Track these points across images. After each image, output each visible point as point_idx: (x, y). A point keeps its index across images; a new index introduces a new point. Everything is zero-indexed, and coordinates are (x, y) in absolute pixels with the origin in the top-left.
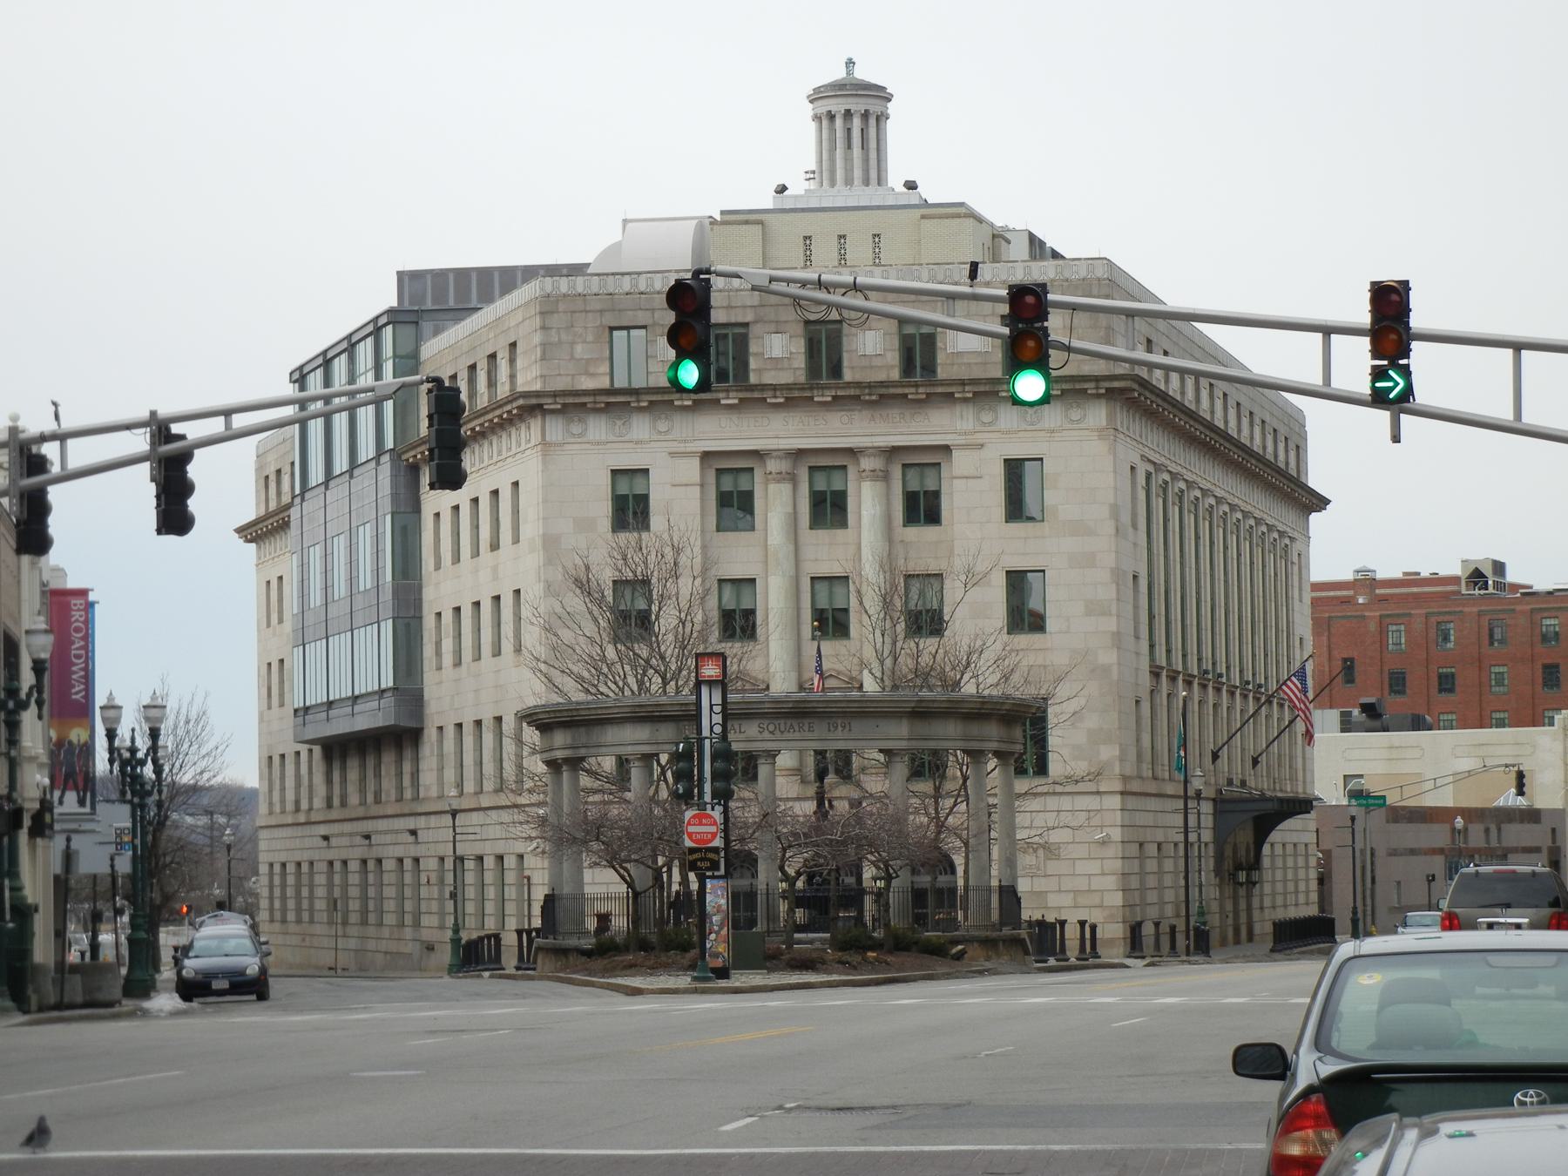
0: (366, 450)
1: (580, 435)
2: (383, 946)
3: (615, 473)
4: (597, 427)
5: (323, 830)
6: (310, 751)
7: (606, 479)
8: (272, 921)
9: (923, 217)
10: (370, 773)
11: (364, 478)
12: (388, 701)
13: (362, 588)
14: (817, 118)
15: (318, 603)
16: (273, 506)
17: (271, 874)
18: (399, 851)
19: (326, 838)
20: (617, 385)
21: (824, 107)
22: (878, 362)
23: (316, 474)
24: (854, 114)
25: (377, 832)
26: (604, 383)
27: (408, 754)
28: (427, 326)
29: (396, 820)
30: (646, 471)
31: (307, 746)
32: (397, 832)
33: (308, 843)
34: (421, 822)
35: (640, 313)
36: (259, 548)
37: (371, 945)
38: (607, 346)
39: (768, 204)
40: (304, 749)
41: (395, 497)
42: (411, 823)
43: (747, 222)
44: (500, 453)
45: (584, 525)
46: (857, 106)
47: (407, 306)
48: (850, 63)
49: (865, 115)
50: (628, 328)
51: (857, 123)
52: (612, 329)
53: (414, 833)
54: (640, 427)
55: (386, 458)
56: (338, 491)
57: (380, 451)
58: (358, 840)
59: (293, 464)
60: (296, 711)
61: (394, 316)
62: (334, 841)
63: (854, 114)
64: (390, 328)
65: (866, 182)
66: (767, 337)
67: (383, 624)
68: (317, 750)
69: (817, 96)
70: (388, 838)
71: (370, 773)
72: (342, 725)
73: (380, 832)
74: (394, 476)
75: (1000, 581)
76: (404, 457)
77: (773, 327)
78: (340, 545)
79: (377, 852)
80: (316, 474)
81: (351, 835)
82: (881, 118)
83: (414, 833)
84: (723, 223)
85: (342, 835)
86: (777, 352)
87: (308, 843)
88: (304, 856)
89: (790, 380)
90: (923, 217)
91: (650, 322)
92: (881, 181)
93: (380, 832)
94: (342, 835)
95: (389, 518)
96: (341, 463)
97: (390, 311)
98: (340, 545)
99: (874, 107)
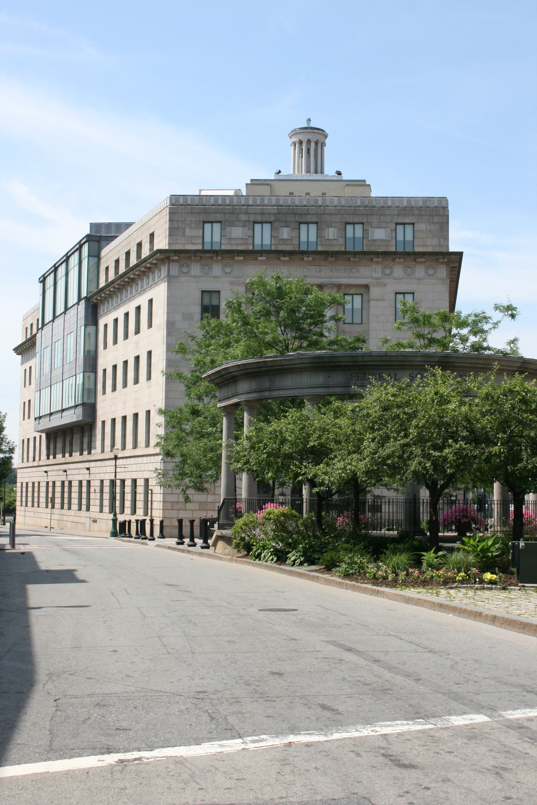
0: (73, 298)
1: (187, 273)
2: (71, 518)
3: (203, 292)
4: (196, 269)
5: (45, 468)
6: (41, 436)
7: (198, 295)
8: (21, 505)
9: (347, 185)
10: (68, 444)
11: (72, 313)
12: (80, 410)
13: (68, 361)
14: (294, 144)
15: (47, 372)
16: (29, 336)
17: (22, 487)
18: (80, 478)
19: (46, 472)
20: (205, 248)
21: (295, 139)
22: (334, 243)
23: (49, 317)
24: (311, 142)
25: (69, 469)
26: (200, 247)
27: (86, 434)
28: (103, 243)
29: (79, 464)
30: (219, 292)
31: (39, 434)
32: (80, 469)
33: (38, 474)
34: (92, 464)
35: (218, 215)
36: (22, 357)
37: (65, 518)
38: (202, 230)
39: (273, 178)
40: (37, 435)
41: (86, 317)
42: (87, 465)
43: (263, 184)
44: (142, 287)
45: (187, 317)
46: (313, 138)
47: (93, 234)
48: (309, 120)
49: (316, 143)
50: (212, 222)
51: (313, 145)
52: (204, 222)
53: (88, 469)
54: (217, 269)
55: (83, 303)
56: (59, 321)
57: (80, 299)
58: (61, 473)
59: (38, 320)
60: (35, 419)
61: (89, 238)
62: (49, 473)
63: (311, 142)
64: (87, 244)
65: (316, 172)
66: (280, 228)
67: (78, 376)
68: (44, 435)
69: (294, 133)
70: (75, 472)
71: (68, 444)
72: (57, 421)
73: (71, 469)
74: (86, 308)
75: (99, 481)
76: (91, 300)
77: (283, 224)
78: (59, 346)
79: (70, 478)
80: (49, 317)
81: (58, 470)
82: (323, 145)
83: (88, 469)
84: (251, 184)
85: (53, 471)
86: (285, 236)
87: (38, 474)
88: (36, 480)
89: (292, 249)
90: (347, 185)
91: (223, 219)
92: (322, 172)
93: (71, 469)
94: (53, 471)
95: (83, 328)
96: (60, 308)
97: (87, 236)
98: (59, 346)
99: (320, 138)
